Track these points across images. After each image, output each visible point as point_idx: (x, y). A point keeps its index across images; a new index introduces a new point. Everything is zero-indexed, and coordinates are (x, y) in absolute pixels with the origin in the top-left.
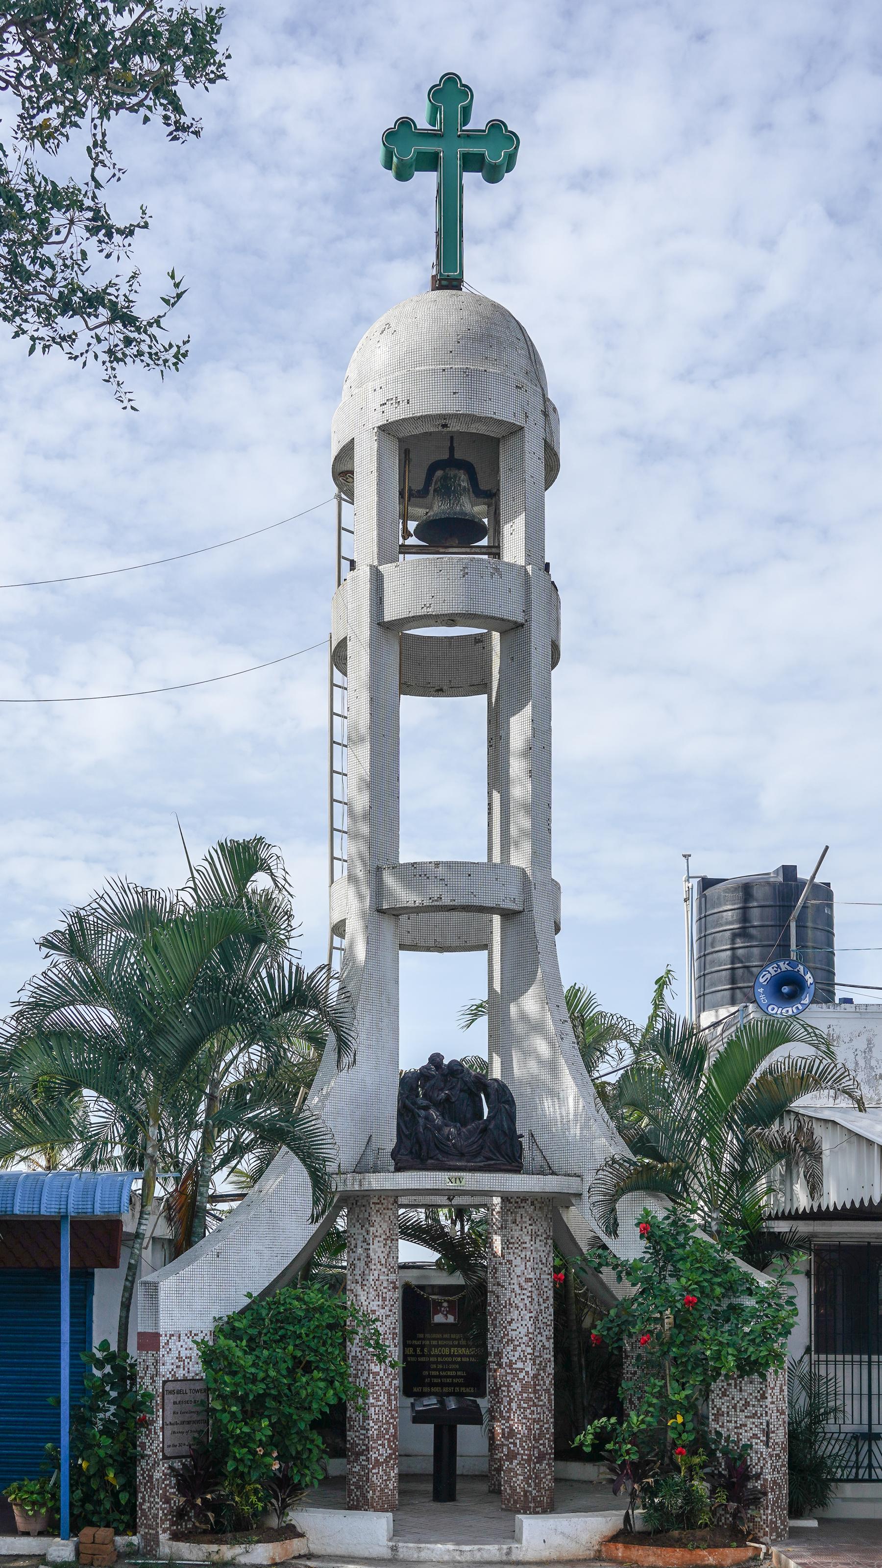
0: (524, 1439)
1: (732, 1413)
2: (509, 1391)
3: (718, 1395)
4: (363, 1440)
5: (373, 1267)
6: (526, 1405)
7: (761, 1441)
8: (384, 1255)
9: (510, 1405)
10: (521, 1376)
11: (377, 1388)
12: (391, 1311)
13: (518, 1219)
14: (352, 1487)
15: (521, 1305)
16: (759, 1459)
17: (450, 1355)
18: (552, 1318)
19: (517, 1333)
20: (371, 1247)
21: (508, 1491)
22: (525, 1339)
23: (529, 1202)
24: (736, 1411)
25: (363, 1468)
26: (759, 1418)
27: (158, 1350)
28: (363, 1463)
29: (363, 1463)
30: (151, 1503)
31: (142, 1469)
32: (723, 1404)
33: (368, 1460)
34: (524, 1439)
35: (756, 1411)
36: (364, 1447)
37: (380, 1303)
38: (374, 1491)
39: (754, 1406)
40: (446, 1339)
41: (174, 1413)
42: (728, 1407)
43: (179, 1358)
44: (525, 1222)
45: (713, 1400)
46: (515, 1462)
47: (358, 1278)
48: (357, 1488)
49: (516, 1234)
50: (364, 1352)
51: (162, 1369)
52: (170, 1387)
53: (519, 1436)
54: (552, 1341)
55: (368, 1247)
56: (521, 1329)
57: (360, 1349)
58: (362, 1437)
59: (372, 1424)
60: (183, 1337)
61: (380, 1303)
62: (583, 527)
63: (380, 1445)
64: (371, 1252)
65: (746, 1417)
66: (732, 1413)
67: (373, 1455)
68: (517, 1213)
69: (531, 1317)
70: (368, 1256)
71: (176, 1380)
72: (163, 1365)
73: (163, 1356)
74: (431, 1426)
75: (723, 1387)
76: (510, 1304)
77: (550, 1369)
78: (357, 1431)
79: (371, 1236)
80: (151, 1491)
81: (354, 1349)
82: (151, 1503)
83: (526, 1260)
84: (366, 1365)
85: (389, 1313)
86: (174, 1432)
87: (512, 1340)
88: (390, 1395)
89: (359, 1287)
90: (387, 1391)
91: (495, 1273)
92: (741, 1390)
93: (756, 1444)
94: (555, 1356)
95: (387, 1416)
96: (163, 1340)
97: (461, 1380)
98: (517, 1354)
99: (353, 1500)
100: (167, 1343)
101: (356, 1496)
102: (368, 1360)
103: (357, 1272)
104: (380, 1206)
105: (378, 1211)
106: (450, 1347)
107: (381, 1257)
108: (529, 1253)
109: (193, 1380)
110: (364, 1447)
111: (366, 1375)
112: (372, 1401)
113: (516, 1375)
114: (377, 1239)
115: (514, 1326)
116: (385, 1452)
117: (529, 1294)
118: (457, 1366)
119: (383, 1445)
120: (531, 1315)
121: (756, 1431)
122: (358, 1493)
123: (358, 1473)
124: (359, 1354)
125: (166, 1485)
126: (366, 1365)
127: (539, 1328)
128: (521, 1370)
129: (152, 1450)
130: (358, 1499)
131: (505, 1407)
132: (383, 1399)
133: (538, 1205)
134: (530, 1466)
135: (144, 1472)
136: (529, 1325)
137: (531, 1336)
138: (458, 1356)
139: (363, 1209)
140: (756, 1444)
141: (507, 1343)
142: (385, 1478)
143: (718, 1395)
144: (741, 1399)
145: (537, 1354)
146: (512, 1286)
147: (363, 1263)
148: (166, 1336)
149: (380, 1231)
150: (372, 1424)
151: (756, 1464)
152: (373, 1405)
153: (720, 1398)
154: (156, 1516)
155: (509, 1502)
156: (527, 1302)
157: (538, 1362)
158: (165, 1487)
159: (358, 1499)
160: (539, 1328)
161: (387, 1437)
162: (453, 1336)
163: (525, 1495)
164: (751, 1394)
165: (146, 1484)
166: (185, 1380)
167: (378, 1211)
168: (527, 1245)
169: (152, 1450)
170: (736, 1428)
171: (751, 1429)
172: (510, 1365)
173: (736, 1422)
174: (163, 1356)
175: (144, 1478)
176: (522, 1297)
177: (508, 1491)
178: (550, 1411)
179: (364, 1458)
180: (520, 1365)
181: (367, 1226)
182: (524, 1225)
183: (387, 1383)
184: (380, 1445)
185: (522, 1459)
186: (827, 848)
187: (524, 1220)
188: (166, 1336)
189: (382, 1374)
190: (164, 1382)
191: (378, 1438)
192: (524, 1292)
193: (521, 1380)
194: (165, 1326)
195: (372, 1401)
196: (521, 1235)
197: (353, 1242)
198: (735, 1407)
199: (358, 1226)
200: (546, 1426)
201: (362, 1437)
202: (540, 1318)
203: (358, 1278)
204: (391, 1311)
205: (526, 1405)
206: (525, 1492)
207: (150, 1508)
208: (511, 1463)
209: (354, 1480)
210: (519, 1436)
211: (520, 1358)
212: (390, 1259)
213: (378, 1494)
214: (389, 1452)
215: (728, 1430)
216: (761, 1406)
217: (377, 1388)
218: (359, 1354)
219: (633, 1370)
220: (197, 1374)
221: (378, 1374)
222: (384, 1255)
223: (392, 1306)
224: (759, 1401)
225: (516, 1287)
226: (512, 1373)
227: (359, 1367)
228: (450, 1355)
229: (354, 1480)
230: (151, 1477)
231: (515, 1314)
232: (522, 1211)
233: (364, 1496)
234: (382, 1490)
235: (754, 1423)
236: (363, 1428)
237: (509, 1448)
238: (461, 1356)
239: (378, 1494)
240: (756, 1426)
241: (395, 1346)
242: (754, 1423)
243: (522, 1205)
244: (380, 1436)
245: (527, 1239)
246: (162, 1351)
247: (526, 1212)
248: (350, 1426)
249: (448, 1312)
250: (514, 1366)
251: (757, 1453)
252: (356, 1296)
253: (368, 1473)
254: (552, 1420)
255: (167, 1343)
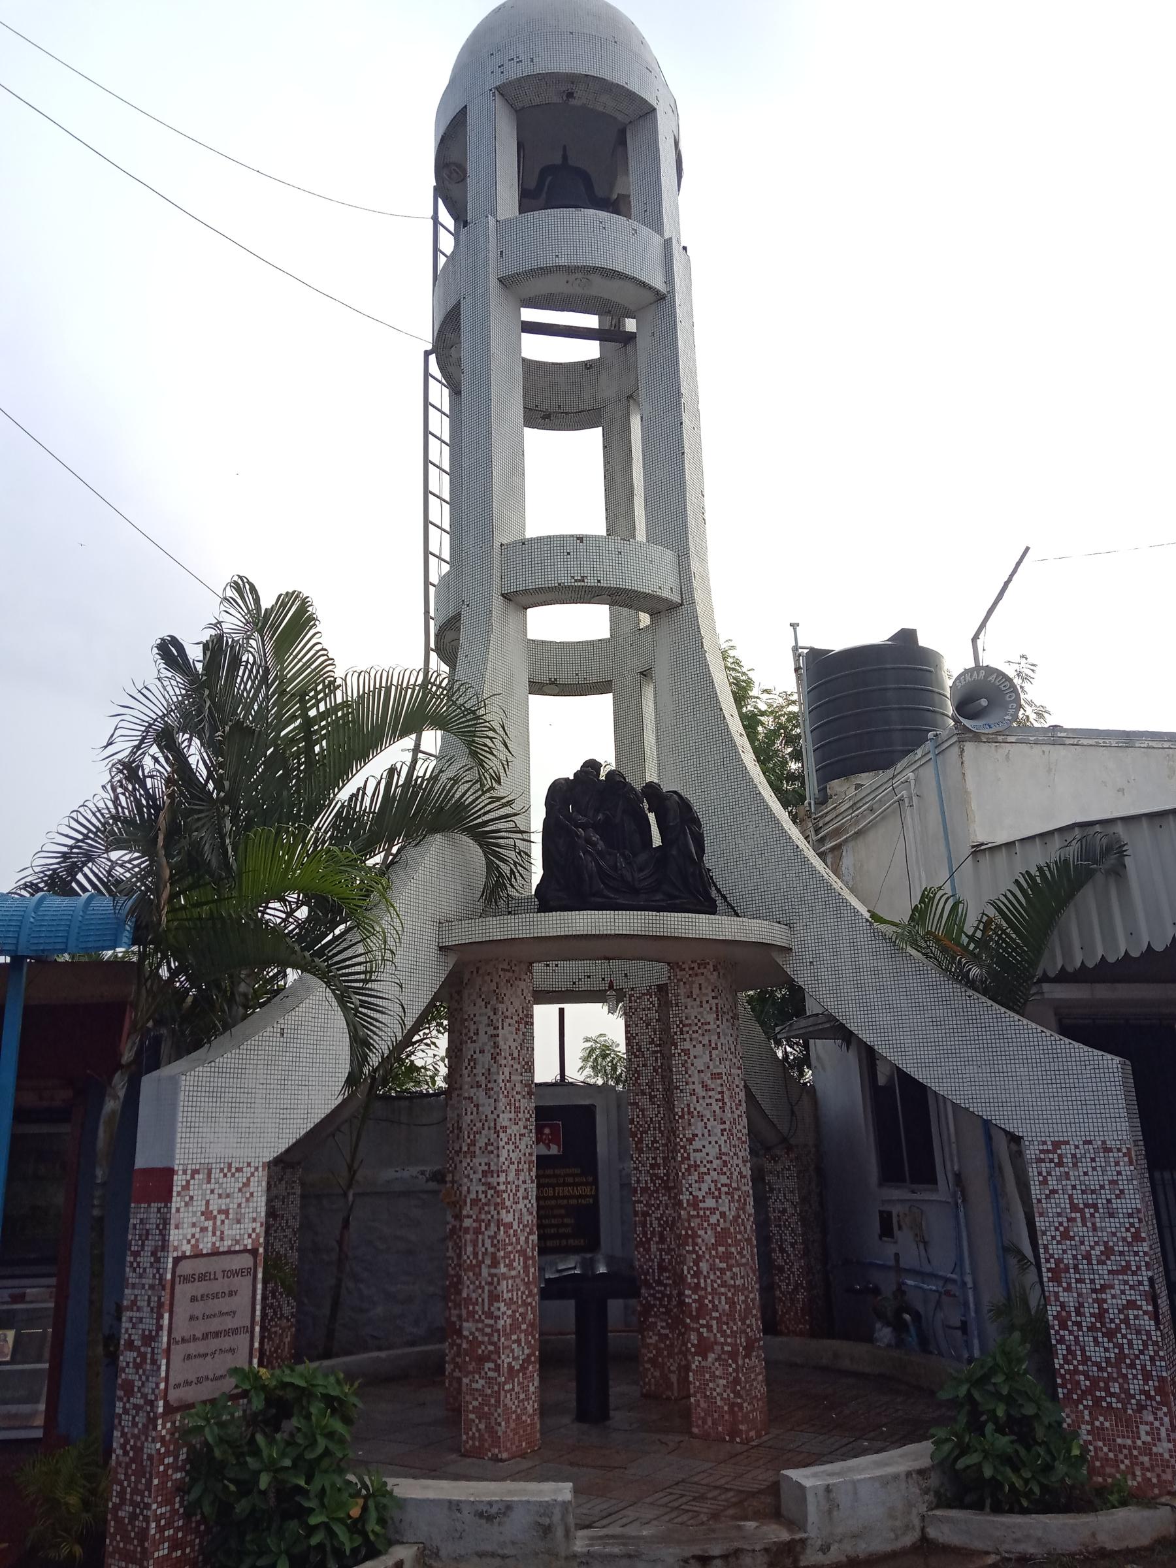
0: (724, 1319)
1: (1083, 1265)
2: (695, 1244)
3: (1053, 1237)
4: (490, 1335)
5: (503, 1062)
6: (724, 1265)
7: (1145, 1313)
8: (516, 1044)
9: (697, 1265)
10: (713, 1220)
11: (510, 1248)
12: (525, 1127)
13: (696, 991)
14: (472, 1416)
15: (708, 1114)
16: (1145, 1344)
17: (554, 1197)
18: (746, 1131)
19: (703, 1154)
20: (500, 1032)
21: (703, 1404)
22: (716, 1163)
23: (711, 967)
24: (1090, 1263)
25: (490, 1382)
26: (1134, 1273)
27: (168, 1198)
28: (491, 1374)
29: (491, 1374)
30: (135, 1504)
31: (123, 1434)
32: (1064, 1252)
33: (497, 1368)
34: (724, 1319)
35: (1128, 1262)
36: (491, 1348)
37: (512, 1115)
38: (508, 1422)
39: (1121, 1253)
40: (549, 1176)
41: (191, 1318)
42: (1075, 1257)
43: (207, 1214)
44: (707, 995)
45: (1046, 1248)
46: (711, 1356)
47: (481, 1079)
48: (480, 1418)
49: (693, 1012)
50: (491, 1192)
51: (175, 1236)
52: (185, 1268)
53: (715, 1314)
54: (749, 1165)
55: (495, 1032)
56: (708, 1149)
57: (483, 1188)
58: (488, 1330)
59: (503, 1309)
60: (216, 1174)
61: (512, 1115)
62: (730, 219)
63: (514, 1342)
64: (500, 1040)
65: (1110, 1272)
66: (1083, 1265)
67: (505, 1360)
68: (693, 982)
69: (723, 1130)
70: (496, 1045)
71: (198, 1255)
72: (177, 1227)
73: (178, 1210)
74: (571, 1303)
75: (193, 1236)
76: (690, 1113)
77: (750, 1209)
78: (480, 1321)
79: (500, 1016)
80: (137, 1482)
81: (473, 1189)
82: (135, 1504)
83: (711, 1047)
84: (494, 1213)
85: (523, 1131)
86: (189, 1357)
87: (696, 1166)
88: (526, 1259)
89: (481, 1093)
90: (522, 1253)
91: (637, 1078)
92: (1095, 1229)
93: (1136, 1317)
94: (753, 1187)
95: (523, 1293)
96: (179, 1181)
97: (569, 1230)
98: (705, 1187)
99: (473, 1438)
100: (186, 1187)
101: (479, 1430)
102: (496, 1205)
103: (479, 1070)
104: (510, 974)
105: (508, 981)
106: (553, 1186)
107: (513, 1048)
108: (714, 1038)
109: (229, 1252)
110: (491, 1348)
111: (493, 1228)
112: (503, 1270)
113: (706, 1218)
114: (508, 1021)
115: (697, 1144)
116: (521, 1352)
117: (720, 1097)
118: (563, 1212)
119: (518, 1341)
120: (722, 1127)
121: (1131, 1295)
122: (482, 1426)
123: (481, 1391)
124: (482, 1196)
125: (168, 1466)
126: (494, 1213)
127: (735, 1146)
128: (713, 1211)
129: (144, 1396)
130: (481, 1435)
131: (690, 1268)
132: (518, 1265)
133: (722, 972)
134: (736, 1363)
135: (127, 1442)
136: (721, 1142)
137: (724, 1158)
138: (564, 1197)
139: (488, 978)
140: (1136, 1317)
141: (688, 1170)
142: (522, 1396)
143: (1053, 1237)
144: (1096, 1243)
145: (734, 1185)
146: (692, 1087)
147: (488, 1056)
148: (185, 1172)
149: (512, 1010)
150: (503, 1309)
151: (1141, 1352)
152: (505, 1277)
153: (1059, 1243)
154: (143, 1534)
155: (704, 1423)
156: (716, 1107)
157: (736, 1197)
158: (166, 1470)
159: (481, 1435)
160: (735, 1146)
161: (524, 1327)
162: (557, 1172)
163: (731, 1411)
164: (1114, 1234)
165: (128, 1466)
166: (215, 1253)
167: (508, 981)
168: (712, 1026)
169: (144, 1396)
170: (1094, 1291)
171: (1123, 1292)
172: (695, 1203)
173: (1092, 1281)
174: (178, 1210)
175: (126, 1453)
176: (709, 1101)
177: (703, 1404)
178: (754, 1272)
179: (492, 1365)
180: (710, 1203)
181: (493, 1002)
182: (704, 999)
183: (522, 1239)
184: (514, 1342)
185: (724, 1352)
186: (1027, 549)
187: (704, 991)
188: (185, 1172)
189: (515, 1226)
190: (177, 1261)
191: (513, 1332)
192: (710, 1093)
193: (713, 1227)
194: (183, 1156)
195: (503, 1270)
196: (699, 1013)
197: (473, 1028)
198: (1087, 1257)
199: (480, 1003)
200: (752, 1296)
201: (488, 1330)
202: (735, 1131)
203: (481, 1079)
204: (525, 1127)
205: (724, 1265)
206: (732, 1405)
207: (133, 1517)
208: (705, 1358)
209: (475, 1403)
210: (715, 1314)
211: (709, 1192)
212: (524, 1052)
213: (513, 1425)
214: (527, 1351)
215: (1080, 1295)
216: (1136, 1254)
217: (510, 1248)
218: (482, 1196)
219: (781, 1207)
220: (237, 1242)
221: (510, 1225)
222: (516, 1044)
223: (527, 1120)
224: (1129, 1244)
225: (698, 1088)
226: (698, 1216)
227: (483, 1217)
228: (554, 1197)
229: (475, 1403)
230: (138, 1450)
231: (698, 1127)
232: (700, 979)
233: (491, 1430)
234: (518, 1417)
235: (1126, 1283)
236: (490, 1315)
237: (700, 1335)
238: (580, 1196)
239: (513, 1425)
240: (1132, 1288)
241: (532, 1182)
242: (1126, 1283)
243: (702, 970)
244: (515, 1327)
245: (711, 1017)
246: (176, 1201)
247: (707, 980)
248: (468, 1312)
249: (550, 1141)
250: (701, 1205)
251: (1138, 1332)
252: (477, 1106)
253: (498, 1393)
254: (757, 1286)
255: (186, 1187)
